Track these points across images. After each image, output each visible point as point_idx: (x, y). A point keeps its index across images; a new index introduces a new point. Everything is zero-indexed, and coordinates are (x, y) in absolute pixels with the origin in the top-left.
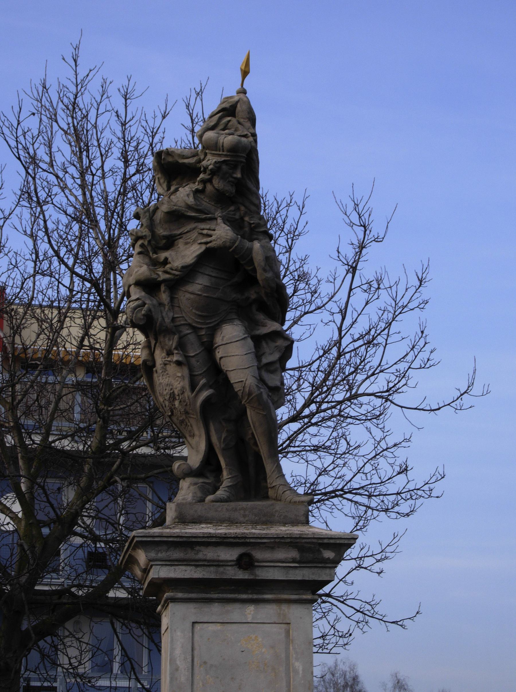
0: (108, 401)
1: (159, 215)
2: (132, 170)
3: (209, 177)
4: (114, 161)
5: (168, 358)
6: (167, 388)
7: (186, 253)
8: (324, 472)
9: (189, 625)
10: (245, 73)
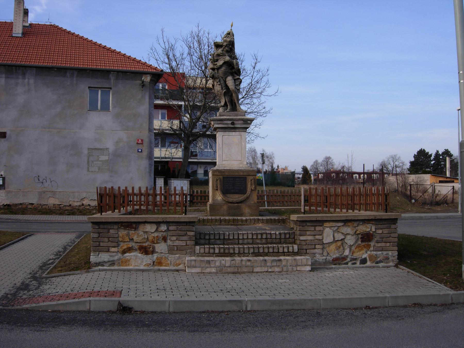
0: (206, 95)
1: (215, 55)
2: (210, 48)
4: (206, 47)
7: (220, 63)
8: (249, 108)
10: (232, 26)
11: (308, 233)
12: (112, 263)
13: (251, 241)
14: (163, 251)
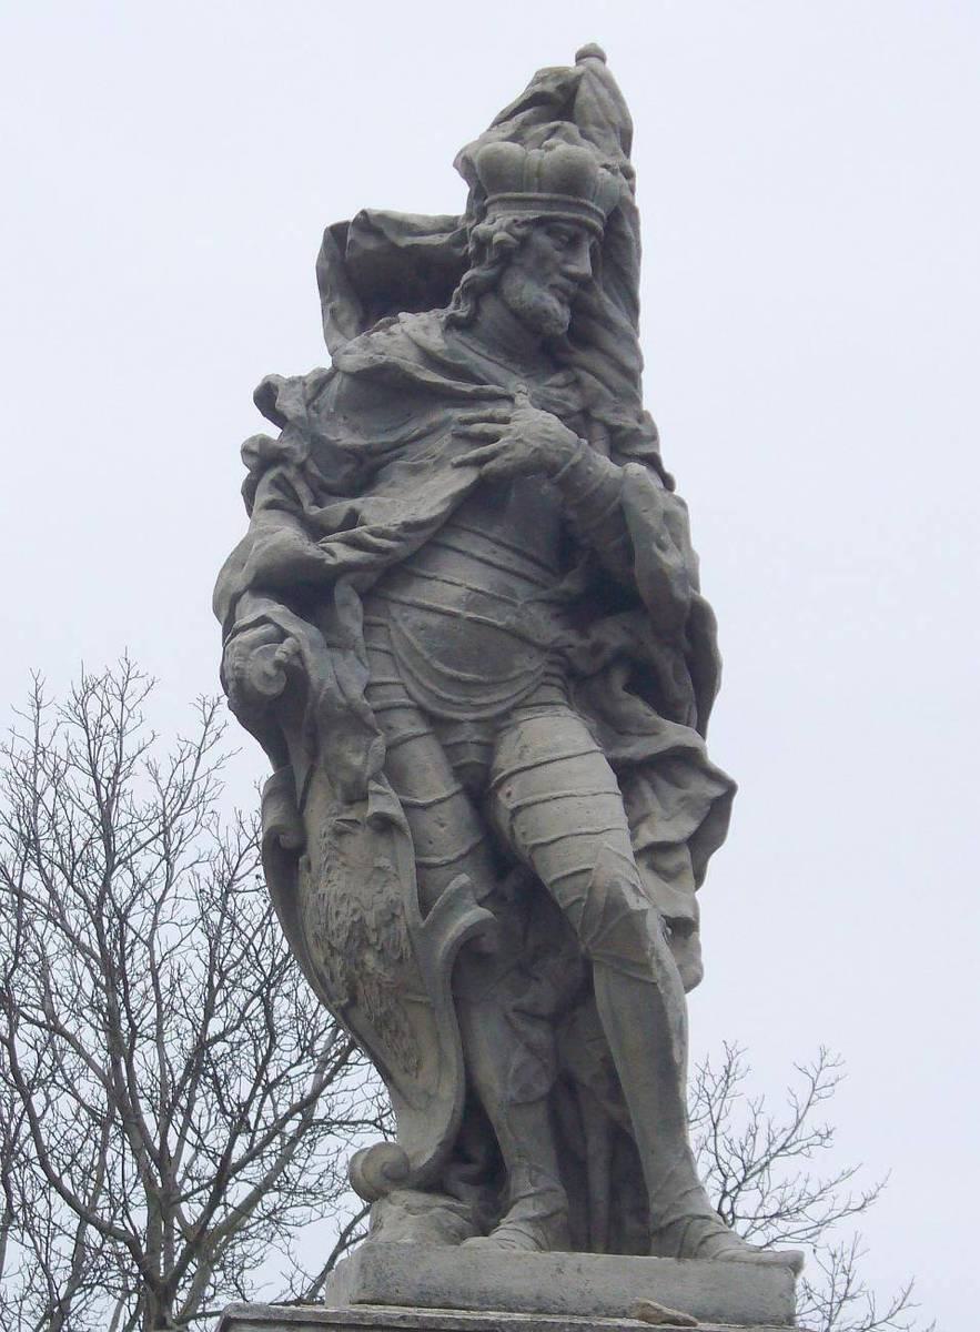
3: (491, 272)
5: (347, 811)
6: (343, 909)
7: (417, 497)
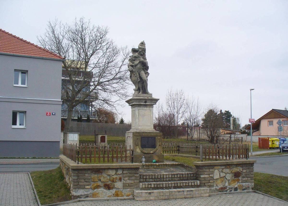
9: (138, 110)
11: (206, 173)
12: (87, 196)
13: (171, 179)
14: (119, 187)
